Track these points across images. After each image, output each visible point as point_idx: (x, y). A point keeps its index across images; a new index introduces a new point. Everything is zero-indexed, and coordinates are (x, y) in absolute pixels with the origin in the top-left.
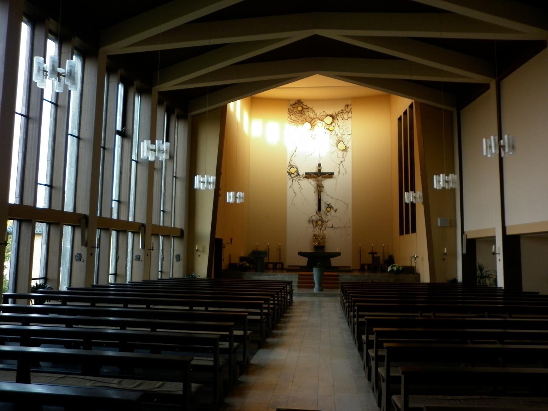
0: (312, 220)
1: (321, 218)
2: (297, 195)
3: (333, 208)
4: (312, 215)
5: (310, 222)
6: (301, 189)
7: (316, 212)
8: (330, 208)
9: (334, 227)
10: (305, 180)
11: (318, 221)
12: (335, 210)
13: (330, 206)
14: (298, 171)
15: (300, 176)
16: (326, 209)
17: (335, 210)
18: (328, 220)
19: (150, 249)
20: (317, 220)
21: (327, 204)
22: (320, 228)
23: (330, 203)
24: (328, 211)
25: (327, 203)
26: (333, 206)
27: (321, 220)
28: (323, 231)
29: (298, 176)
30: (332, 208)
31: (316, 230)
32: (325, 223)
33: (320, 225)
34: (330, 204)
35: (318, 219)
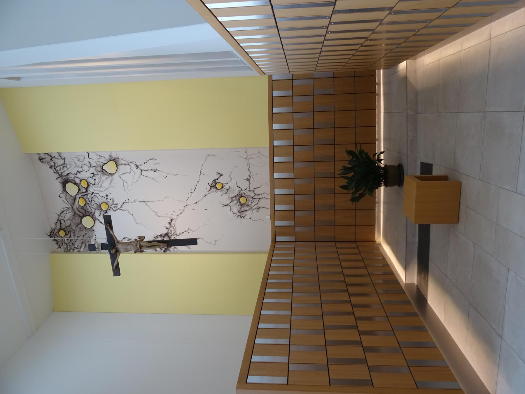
0: (239, 212)
1: (235, 198)
2: (200, 237)
3: (216, 178)
4: (232, 212)
5: (243, 215)
6: (189, 231)
7: (226, 206)
8: (216, 184)
9: (249, 177)
10: (174, 224)
11: (240, 203)
12: (219, 175)
13: (214, 184)
14: (162, 235)
15: (170, 231)
16: (219, 190)
17: (219, 175)
18: (237, 186)
19: (251, 191)
20: (239, 204)
21: (210, 189)
22: (251, 199)
23: (208, 184)
24: (223, 186)
25: (208, 190)
26: (214, 180)
27: (238, 198)
28: (256, 195)
29: (170, 235)
30: (217, 181)
31: (256, 206)
32: (242, 192)
33: (247, 200)
34: (210, 184)
35: (237, 203)
